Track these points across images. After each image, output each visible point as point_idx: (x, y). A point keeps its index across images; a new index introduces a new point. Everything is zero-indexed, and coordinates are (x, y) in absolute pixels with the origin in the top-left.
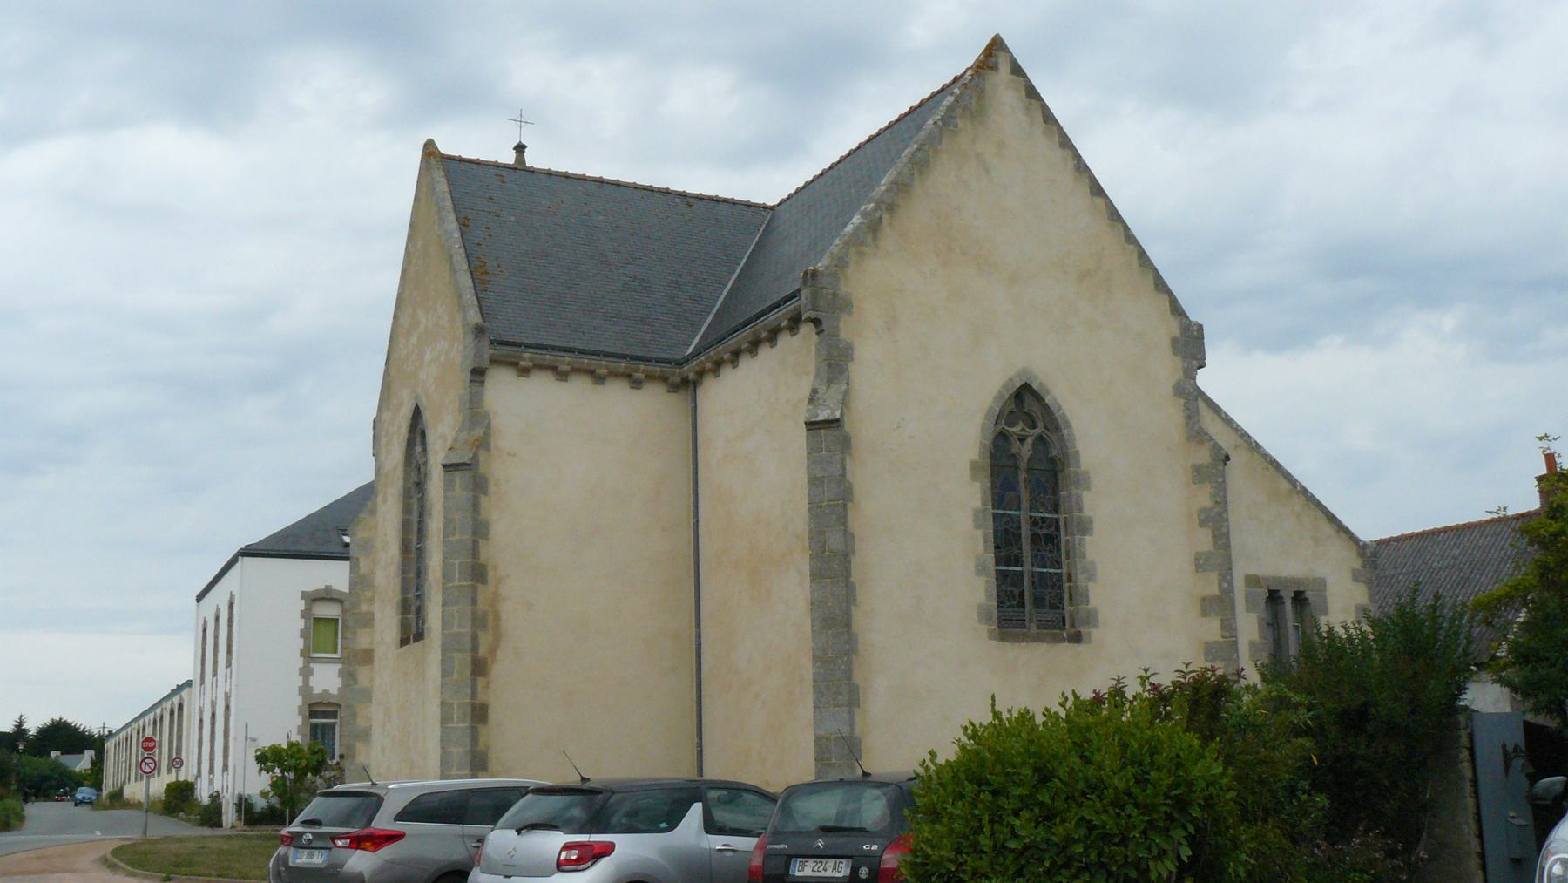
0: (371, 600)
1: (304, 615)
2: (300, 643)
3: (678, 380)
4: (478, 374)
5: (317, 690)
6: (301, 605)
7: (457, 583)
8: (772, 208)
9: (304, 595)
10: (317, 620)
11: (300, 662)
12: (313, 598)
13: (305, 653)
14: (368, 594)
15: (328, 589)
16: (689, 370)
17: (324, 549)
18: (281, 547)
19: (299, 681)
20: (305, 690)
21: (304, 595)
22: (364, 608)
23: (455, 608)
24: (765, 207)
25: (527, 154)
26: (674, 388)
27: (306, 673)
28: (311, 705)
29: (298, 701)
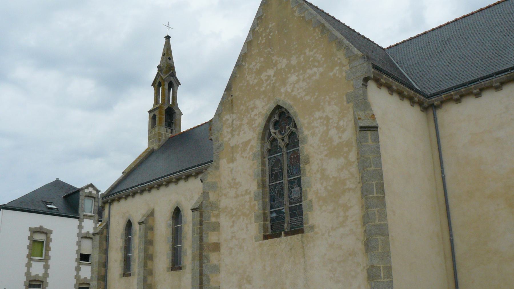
0: (218, 216)
1: (29, 238)
2: (27, 252)
3: (458, 97)
4: (366, 80)
5: (33, 274)
6: (29, 234)
7: (375, 195)
8: (385, 49)
9: (30, 229)
10: (34, 241)
11: (26, 260)
12: (35, 231)
13: (29, 256)
14: (216, 212)
15: (41, 227)
16: (435, 101)
17: (40, 209)
18: (23, 206)
19: (25, 269)
20: (28, 274)
21: (30, 229)
22: (213, 220)
23: (376, 210)
24: (381, 48)
25: (171, 40)
26: (425, 109)
27: (29, 266)
28: (30, 281)
29: (24, 279)
